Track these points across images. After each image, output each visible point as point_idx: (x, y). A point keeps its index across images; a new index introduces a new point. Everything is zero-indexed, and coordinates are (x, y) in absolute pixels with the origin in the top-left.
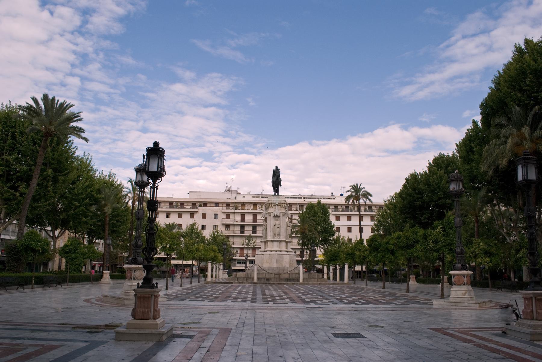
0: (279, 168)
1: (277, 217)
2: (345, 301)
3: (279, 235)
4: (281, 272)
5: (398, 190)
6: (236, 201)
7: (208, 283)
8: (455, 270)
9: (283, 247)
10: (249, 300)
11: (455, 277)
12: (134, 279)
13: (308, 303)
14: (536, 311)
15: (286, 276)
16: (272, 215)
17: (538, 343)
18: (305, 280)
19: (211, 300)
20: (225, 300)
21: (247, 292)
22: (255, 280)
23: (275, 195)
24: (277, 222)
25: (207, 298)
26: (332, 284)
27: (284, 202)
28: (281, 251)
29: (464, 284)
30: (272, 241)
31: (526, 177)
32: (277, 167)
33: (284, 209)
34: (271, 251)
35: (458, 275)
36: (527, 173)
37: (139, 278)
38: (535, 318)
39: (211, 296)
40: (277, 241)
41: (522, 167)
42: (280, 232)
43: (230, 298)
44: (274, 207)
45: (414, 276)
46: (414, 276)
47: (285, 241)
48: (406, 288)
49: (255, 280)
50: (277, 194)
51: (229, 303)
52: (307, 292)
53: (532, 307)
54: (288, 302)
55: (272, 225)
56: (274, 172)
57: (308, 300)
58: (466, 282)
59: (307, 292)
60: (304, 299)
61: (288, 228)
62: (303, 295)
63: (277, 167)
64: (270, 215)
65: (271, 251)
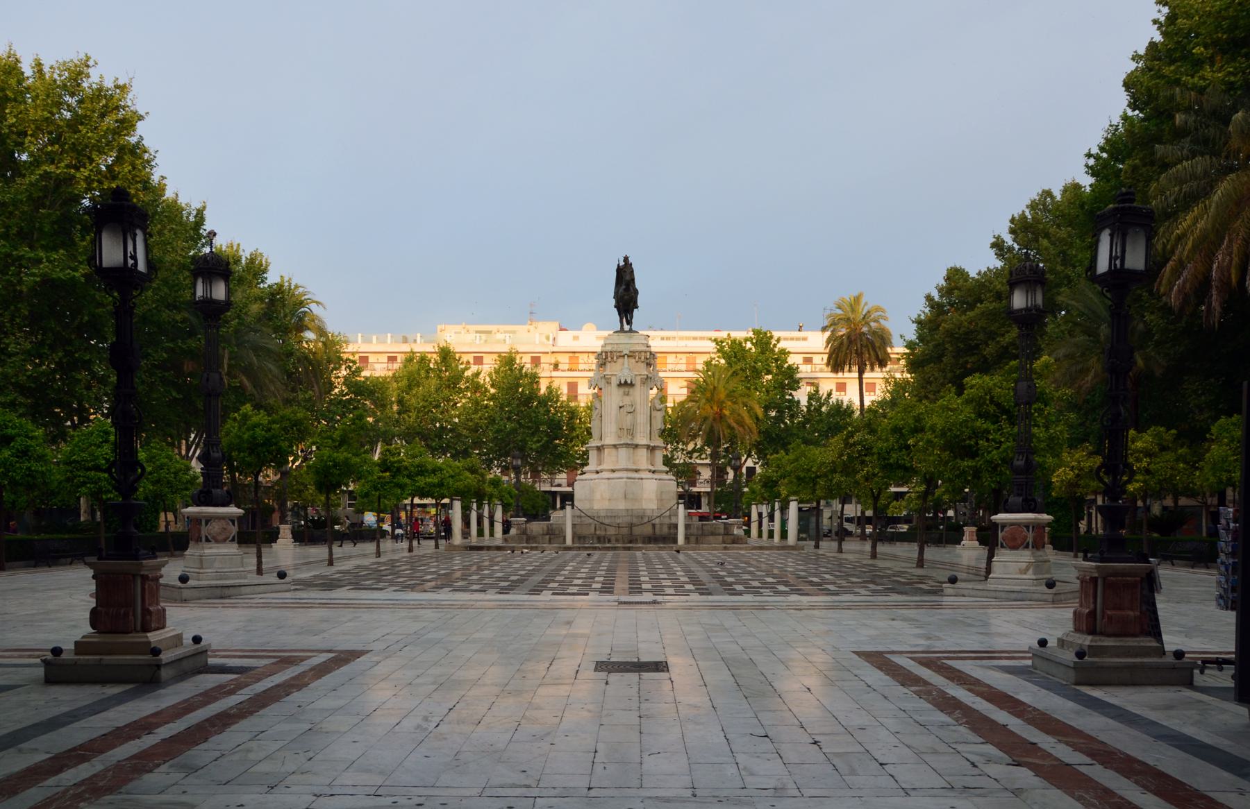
0: (630, 260)
1: (626, 385)
2: (831, 587)
3: (631, 432)
4: (635, 520)
5: (182, 168)
6: (555, 349)
7: (455, 548)
8: (1007, 512)
9: (642, 456)
10: (595, 590)
11: (1006, 529)
12: (207, 540)
13: (740, 593)
14: (1103, 612)
15: (648, 530)
16: (614, 381)
17: (1097, 693)
18: (693, 539)
19: (503, 591)
20: (536, 590)
21: (576, 570)
22: (569, 541)
23: (622, 330)
24: (627, 400)
25: (492, 586)
26: (755, 548)
27: (644, 348)
28: (637, 471)
29: (1027, 547)
30: (615, 446)
31: (1118, 262)
32: (626, 259)
33: (643, 366)
34: (613, 471)
35: (1012, 524)
36: (1123, 252)
37: (220, 538)
38: (1098, 630)
39: (505, 579)
40: (627, 445)
41: (1112, 235)
42: (634, 425)
43: (552, 585)
44: (620, 360)
45: (974, 529)
46: (974, 529)
47: (648, 447)
48: (326, 556)
49: (569, 541)
50: (626, 327)
51: (546, 596)
52: (750, 573)
53: (1095, 602)
54: (690, 591)
55: (615, 407)
56: (620, 271)
57: (739, 588)
58: (1030, 540)
59: (750, 573)
60: (731, 584)
61: (654, 413)
62: (731, 574)
63: (626, 259)
64: (609, 383)
65: (613, 471)
